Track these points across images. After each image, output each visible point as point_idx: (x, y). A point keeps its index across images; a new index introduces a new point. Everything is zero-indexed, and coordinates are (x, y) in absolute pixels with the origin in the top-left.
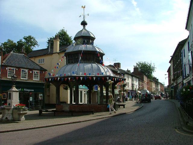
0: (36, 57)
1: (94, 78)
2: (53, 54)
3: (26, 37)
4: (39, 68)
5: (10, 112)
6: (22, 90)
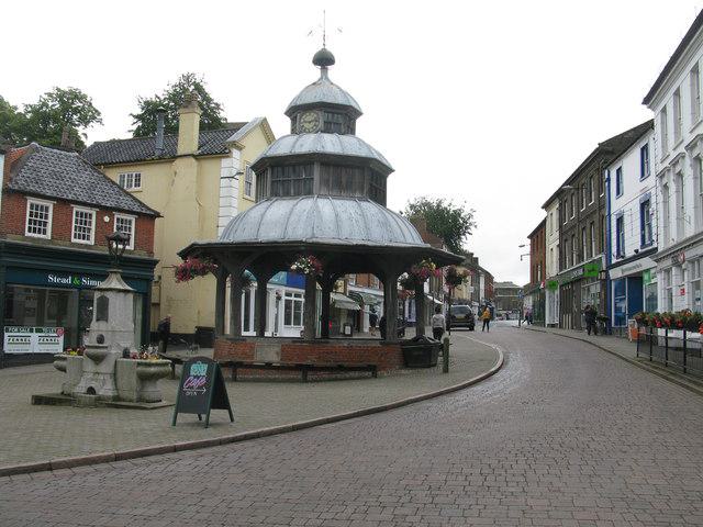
2: (175, 157)
4: (136, 208)
6: (77, 282)
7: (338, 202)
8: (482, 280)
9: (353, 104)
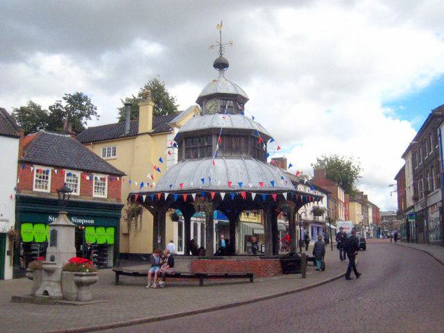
0: (96, 142)
1: (254, 195)
3: (70, 95)
4: (108, 170)
5: (56, 277)
7: (228, 161)
8: (370, 211)
9: (243, 94)
